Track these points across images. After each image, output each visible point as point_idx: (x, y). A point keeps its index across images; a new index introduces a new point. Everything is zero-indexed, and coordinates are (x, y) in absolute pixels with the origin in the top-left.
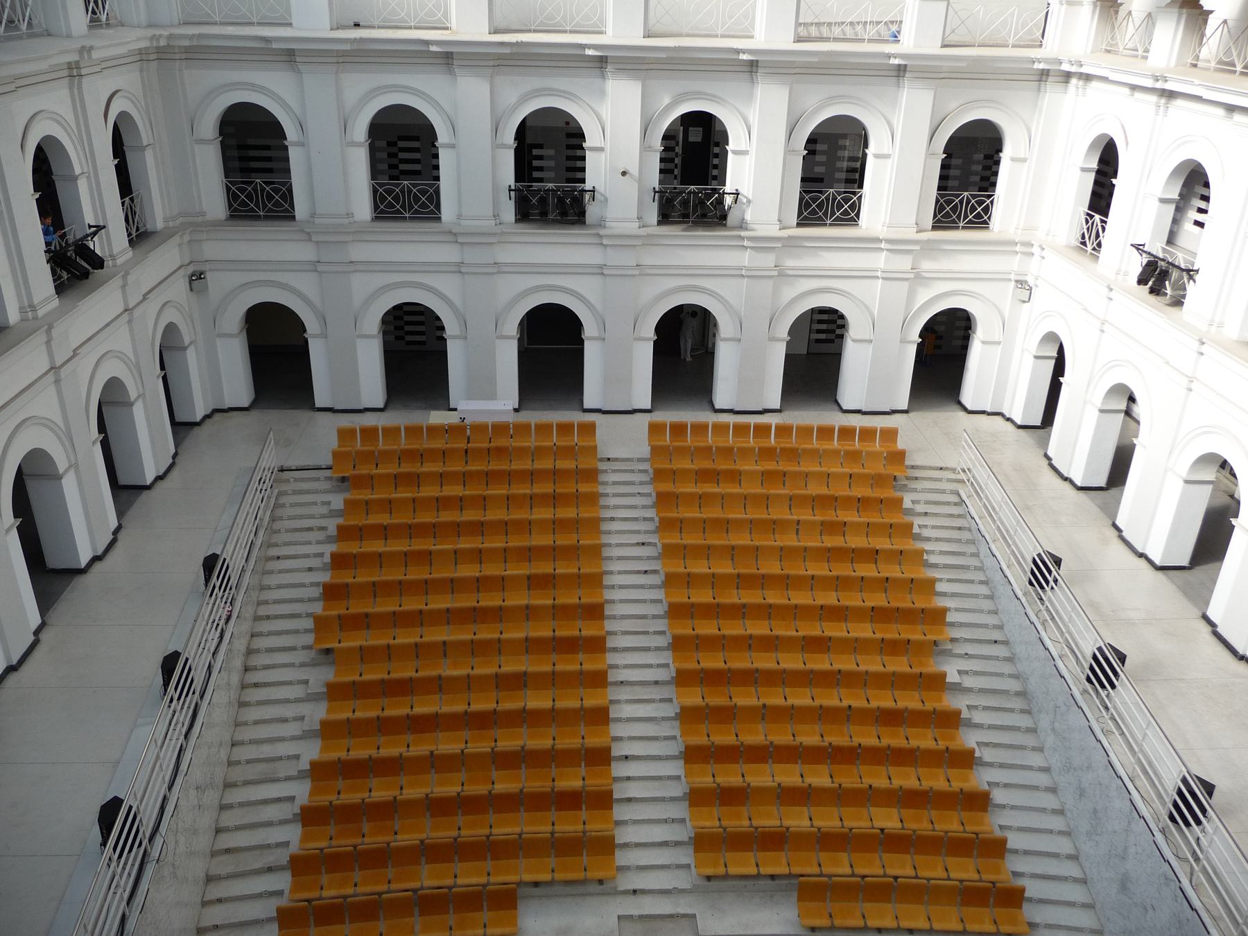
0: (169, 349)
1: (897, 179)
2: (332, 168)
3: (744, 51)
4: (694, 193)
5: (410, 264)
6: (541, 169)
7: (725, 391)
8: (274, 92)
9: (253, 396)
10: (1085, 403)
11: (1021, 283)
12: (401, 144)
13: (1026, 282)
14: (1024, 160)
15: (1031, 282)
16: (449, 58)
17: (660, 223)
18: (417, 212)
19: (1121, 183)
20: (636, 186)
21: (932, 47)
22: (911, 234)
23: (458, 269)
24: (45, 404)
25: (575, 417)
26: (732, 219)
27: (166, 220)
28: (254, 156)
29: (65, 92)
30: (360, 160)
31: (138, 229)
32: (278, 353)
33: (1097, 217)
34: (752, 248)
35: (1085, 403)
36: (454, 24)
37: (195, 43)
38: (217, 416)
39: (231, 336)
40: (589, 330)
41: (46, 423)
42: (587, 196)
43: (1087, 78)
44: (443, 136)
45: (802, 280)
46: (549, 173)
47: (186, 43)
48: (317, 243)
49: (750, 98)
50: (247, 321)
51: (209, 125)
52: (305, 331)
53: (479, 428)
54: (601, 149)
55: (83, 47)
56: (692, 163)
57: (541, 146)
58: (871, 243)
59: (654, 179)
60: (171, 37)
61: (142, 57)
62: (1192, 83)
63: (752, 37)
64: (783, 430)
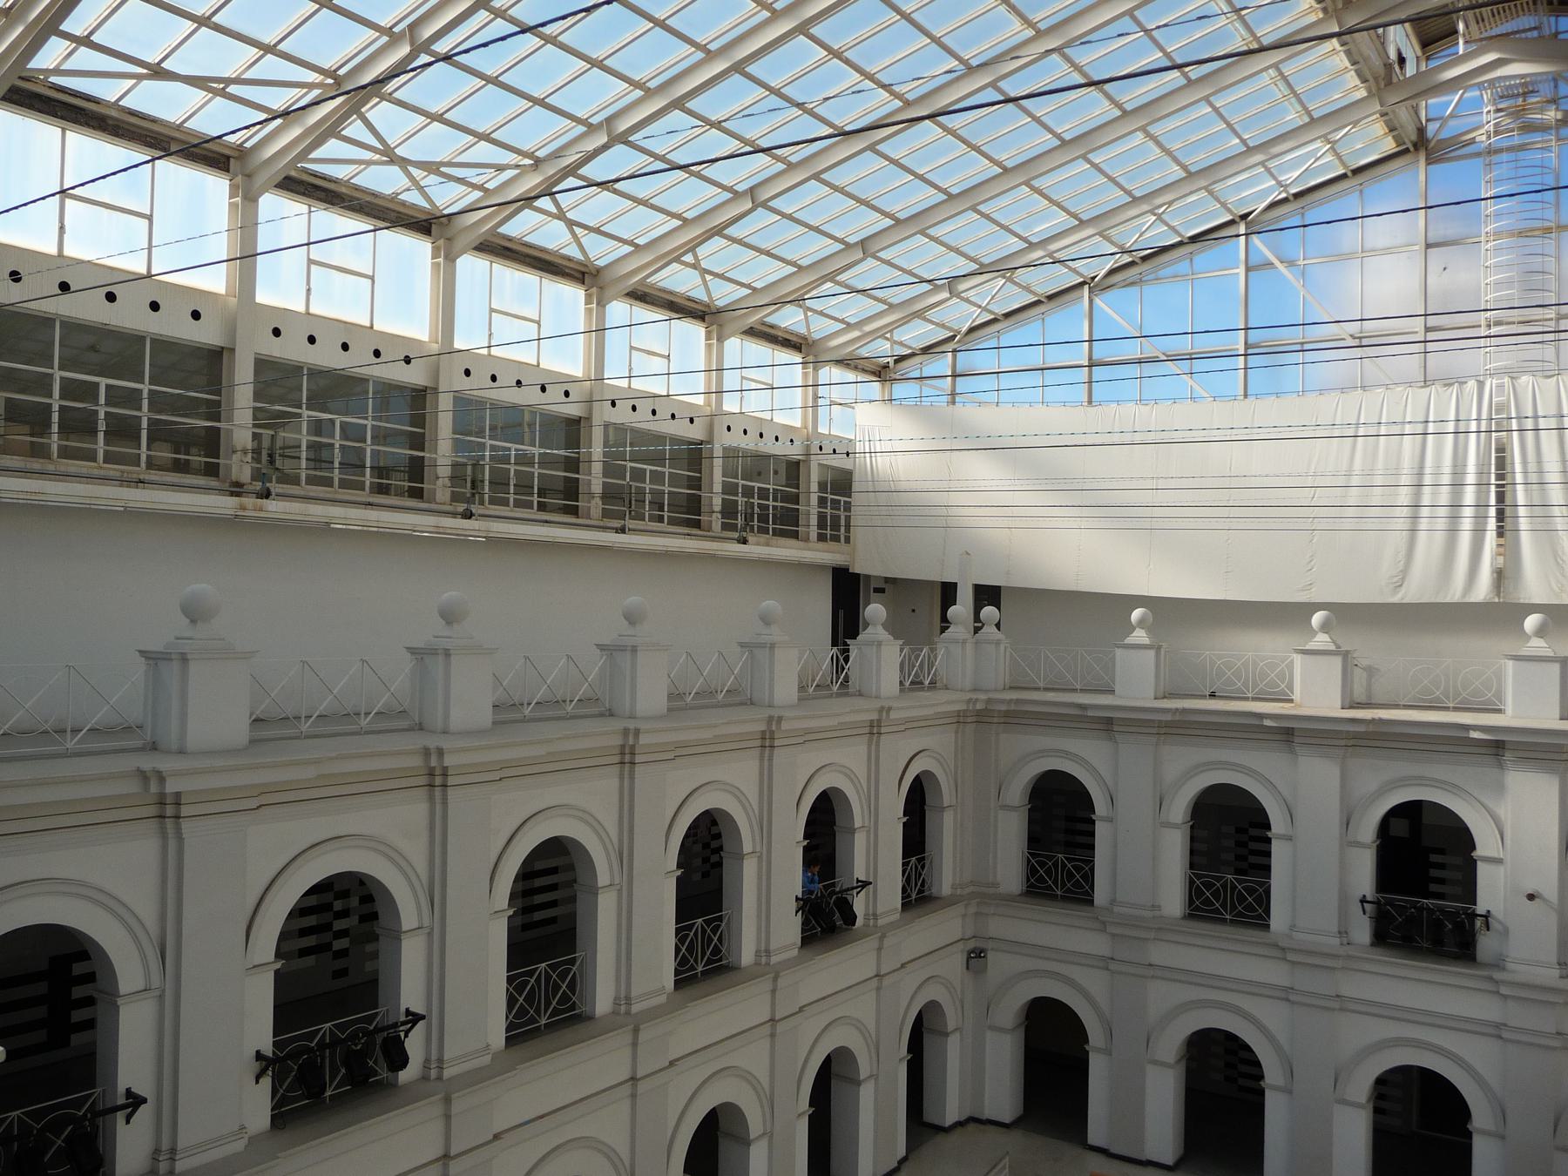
2: (1145, 854)
5: (1226, 985)
6: (1442, 881)
8: (1086, 761)
9: (1019, 1111)
16: (1290, 735)
18: (1240, 914)
23: (1286, 995)
24: (754, 1056)
27: (954, 887)
28: (1061, 826)
29: (863, 749)
31: (920, 892)
32: (1054, 1052)
36: (1297, 696)
37: (1177, 717)
38: (971, 1127)
39: (1001, 1030)
41: (747, 1077)
42: (1478, 923)
47: (1004, 708)
48: (1113, 935)
50: (1027, 1017)
52: (1087, 1041)
54: (1498, 861)
57: (1442, 852)
60: (989, 701)
61: (960, 719)
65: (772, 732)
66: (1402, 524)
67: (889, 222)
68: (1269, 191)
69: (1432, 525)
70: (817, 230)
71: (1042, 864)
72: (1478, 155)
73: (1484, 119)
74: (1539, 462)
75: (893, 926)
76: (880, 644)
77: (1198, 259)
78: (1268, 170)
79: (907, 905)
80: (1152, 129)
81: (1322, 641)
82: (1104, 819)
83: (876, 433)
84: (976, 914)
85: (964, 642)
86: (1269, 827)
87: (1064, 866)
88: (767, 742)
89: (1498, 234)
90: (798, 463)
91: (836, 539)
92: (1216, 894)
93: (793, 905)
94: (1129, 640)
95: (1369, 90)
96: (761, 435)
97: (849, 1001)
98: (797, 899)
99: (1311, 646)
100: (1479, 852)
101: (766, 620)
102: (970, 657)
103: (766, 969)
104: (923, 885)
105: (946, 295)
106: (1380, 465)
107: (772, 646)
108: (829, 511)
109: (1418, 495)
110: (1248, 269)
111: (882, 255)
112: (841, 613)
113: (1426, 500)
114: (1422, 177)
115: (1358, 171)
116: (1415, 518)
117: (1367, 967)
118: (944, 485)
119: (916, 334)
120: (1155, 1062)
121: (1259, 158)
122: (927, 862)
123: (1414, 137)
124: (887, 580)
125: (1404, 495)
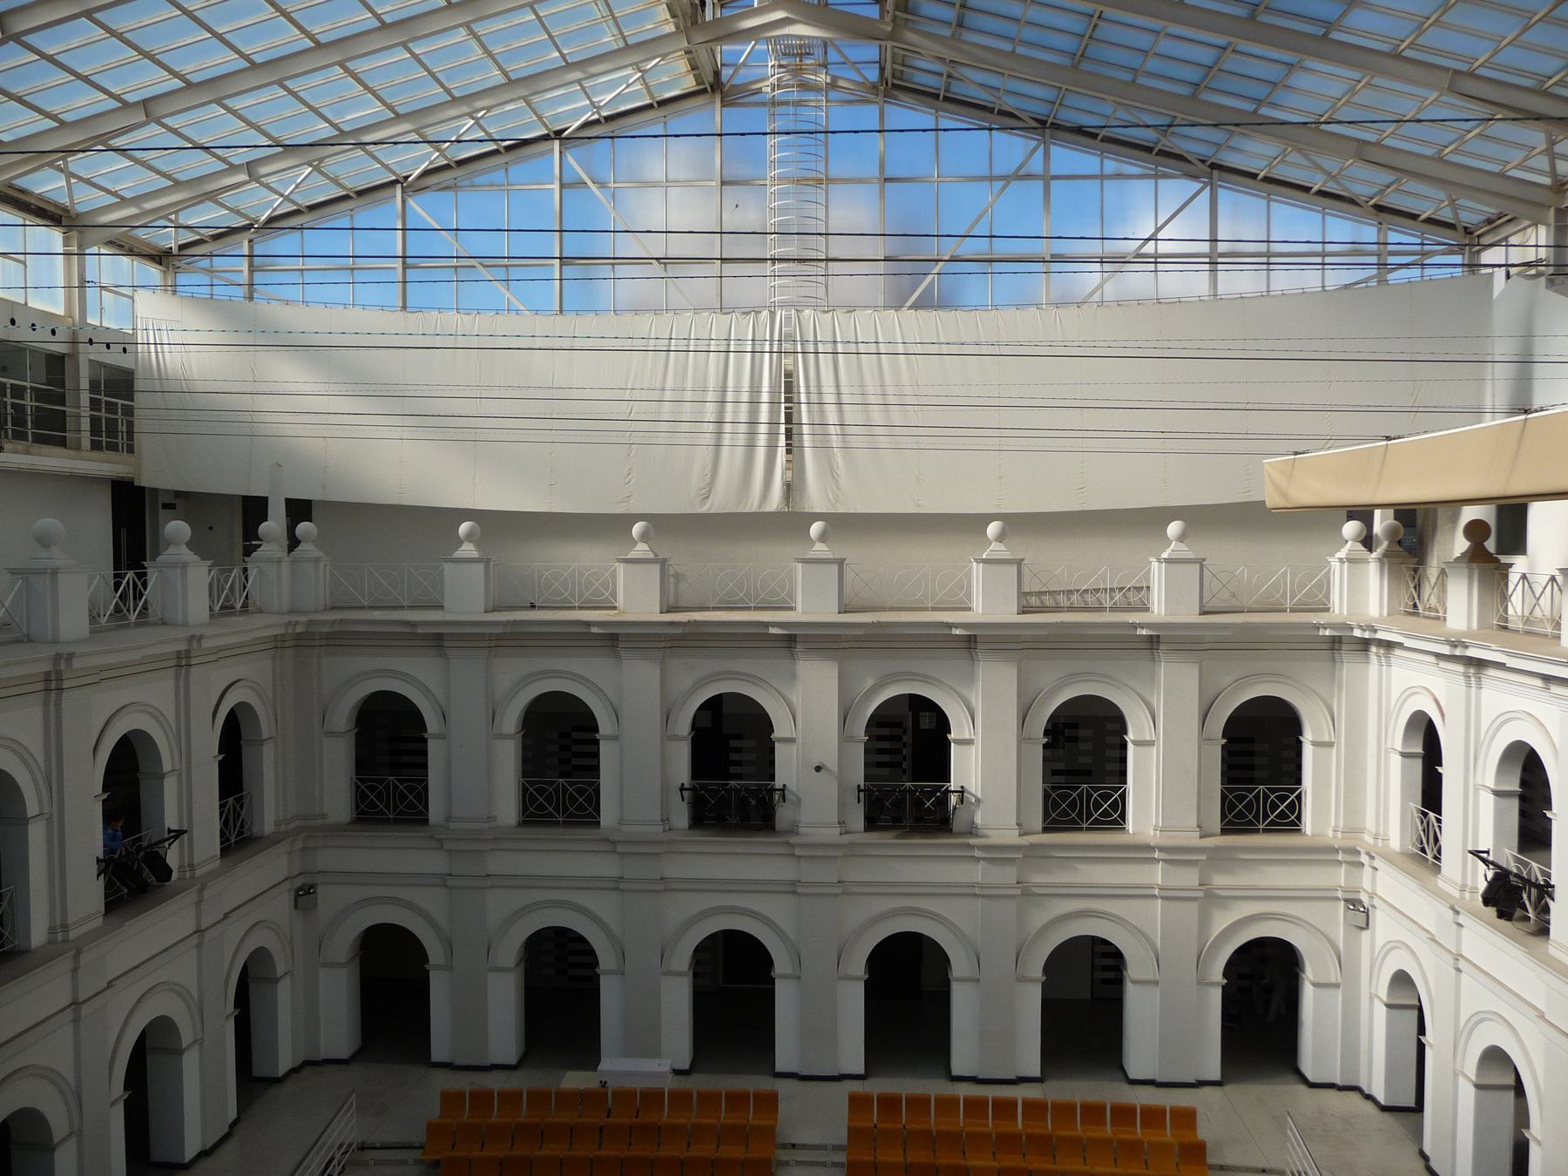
0: (250, 986)
1: (1166, 775)
2: (478, 767)
3: (957, 626)
4: (910, 790)
5: (731, 884)
6: (740, 763)
7: (963, 1057)
8: (416, 679)
10: (1456, 1075)
11: (1354, 903)
12: (575, 735)
13: (1360, 902)
14: (1330, 745)
15: (1364, 897)
16: (615, 640)
17: (867, 829)
18: (572, 815)
19: (1450, 770)
20: (835, 783)
21: (1188, 614)
22: (1193, 839)
23: (616, 885)
25: (933, 1087)
26: (958, 822)
27: (277, 823)
28: (390, 746)
29: (169, 684)
30: (508, 758)
31: (240, 833)
32: (392, 979)
33: (1432, 815)
34: (1348, 863)
35: (1456, 1075)
36: (620, 601)
37: (336, 628)
38: (307, 1071)
39: (505, 970)
40: (781, 965)
43: (1389, 645)
44: (605, 726)
45: (1055, 900)
46: (730, 765)
47: (326, 629)
48: (450, 851)
49: (970, 678)
51: (343, 716)
52: (426, 959)
53: (625, 1096)
54: (792, 740)
55: (193, 637)
56: (906, 762)
57: (739, 737)
58: (1142, 852)
59: (858, 776)
60: (310, 623)
61: (277, 644)
62: (1488, 648)
63: (969, 609)
64: (1034, 1109)
65: (59, 672)
66: (709, 439)
67: (177, 83)
68: (583, 110)
69: (733, 437)
70: (85, 79)
71: (372, 789)
72: (763, 104)
73: (769, 75)
74: (819, 386)
75: (213, 875)
76: (184, 566)
77: (513, 170)
78: (583, 88)
79: (226, 850)
80: (476, 28)
81: (641, 550)
82: (607, 738)
83: (165, 328)
84: (303, 849)
85: (279, 561)
86: (596, 729)
87: (396, 788)
88: (52, 685)
89: (782, 179)
90: (61, 358)
91: (113, 447)
92: (549, 799)
93: (94, 869)
94: (458, 554)
95: (677, 27)
96: (13, 322)
97: (165, 966)
98: (98, 860)
99: (632, 555)
100: (777, 734)
101: (44, 541)
102: (282, 578)
103: (64, 945)
104: (242, 826)
105: (243, 177)
106: (689, 385)
107: (55, 572)
108: (103, 414)
109: (721, 412)
110: (562, 186)
111: (167, 121)
112: (123, 531)
113: (728, 418)
114: (718, 118)
115: (663, 103)
116: (720, 433)
117: (689, 849)
118: (248, 388)
119: (208, 216)
120: (497, 969)
121: (577, 75)
122: (246, 802)
123: (711, 79)
124: (178, 494)
125: (710, 412)
